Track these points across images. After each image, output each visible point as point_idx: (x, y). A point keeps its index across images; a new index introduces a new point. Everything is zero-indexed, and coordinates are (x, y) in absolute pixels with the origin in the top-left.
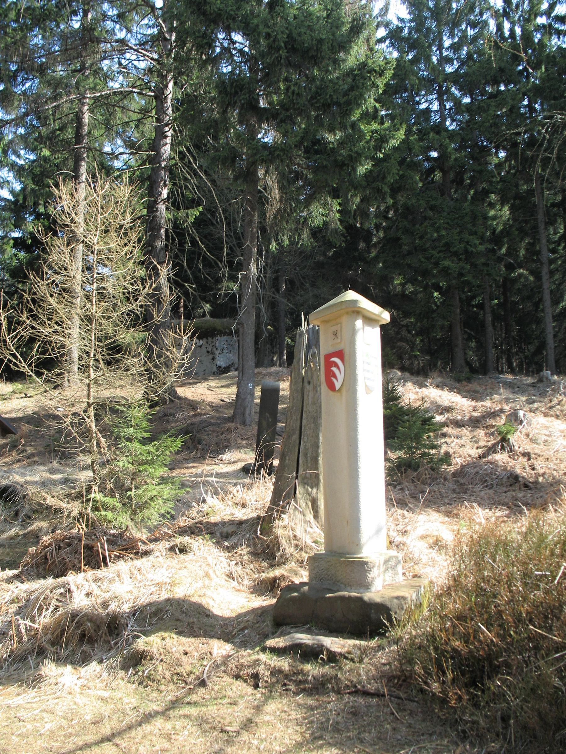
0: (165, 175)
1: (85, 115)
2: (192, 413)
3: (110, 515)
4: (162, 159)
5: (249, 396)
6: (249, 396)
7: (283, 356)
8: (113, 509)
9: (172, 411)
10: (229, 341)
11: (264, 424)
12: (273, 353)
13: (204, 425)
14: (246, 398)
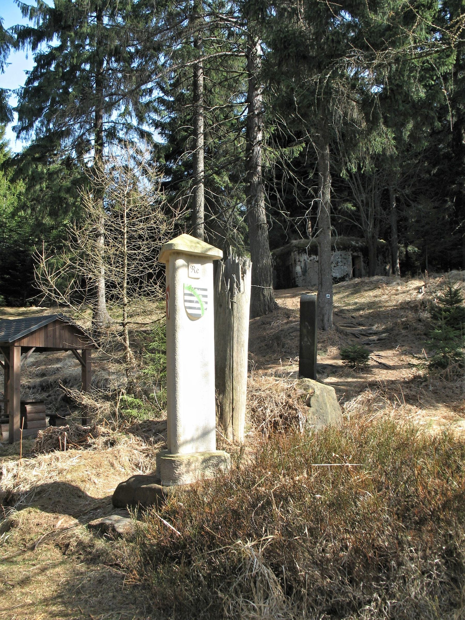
0: (259, 122)
1: (200, 78)
2: (285, 321)
3: (134, 412)
4: (255, 108)
5: (327, 305)
6: (327, 305)
7: (396, 264)
8: (139, 407)
9: (269, 320)
10: (343, 255)
11: (305, 331)
12: (386, 263)
13: (290, 331)
14: (324, 307)
